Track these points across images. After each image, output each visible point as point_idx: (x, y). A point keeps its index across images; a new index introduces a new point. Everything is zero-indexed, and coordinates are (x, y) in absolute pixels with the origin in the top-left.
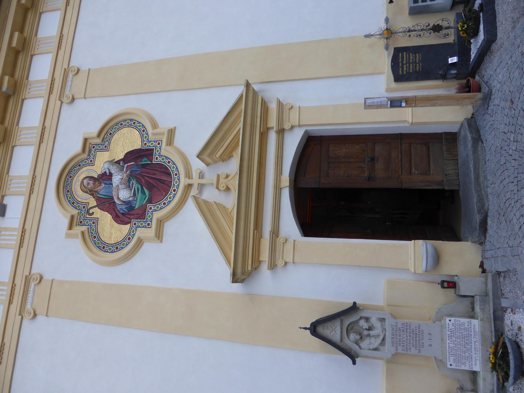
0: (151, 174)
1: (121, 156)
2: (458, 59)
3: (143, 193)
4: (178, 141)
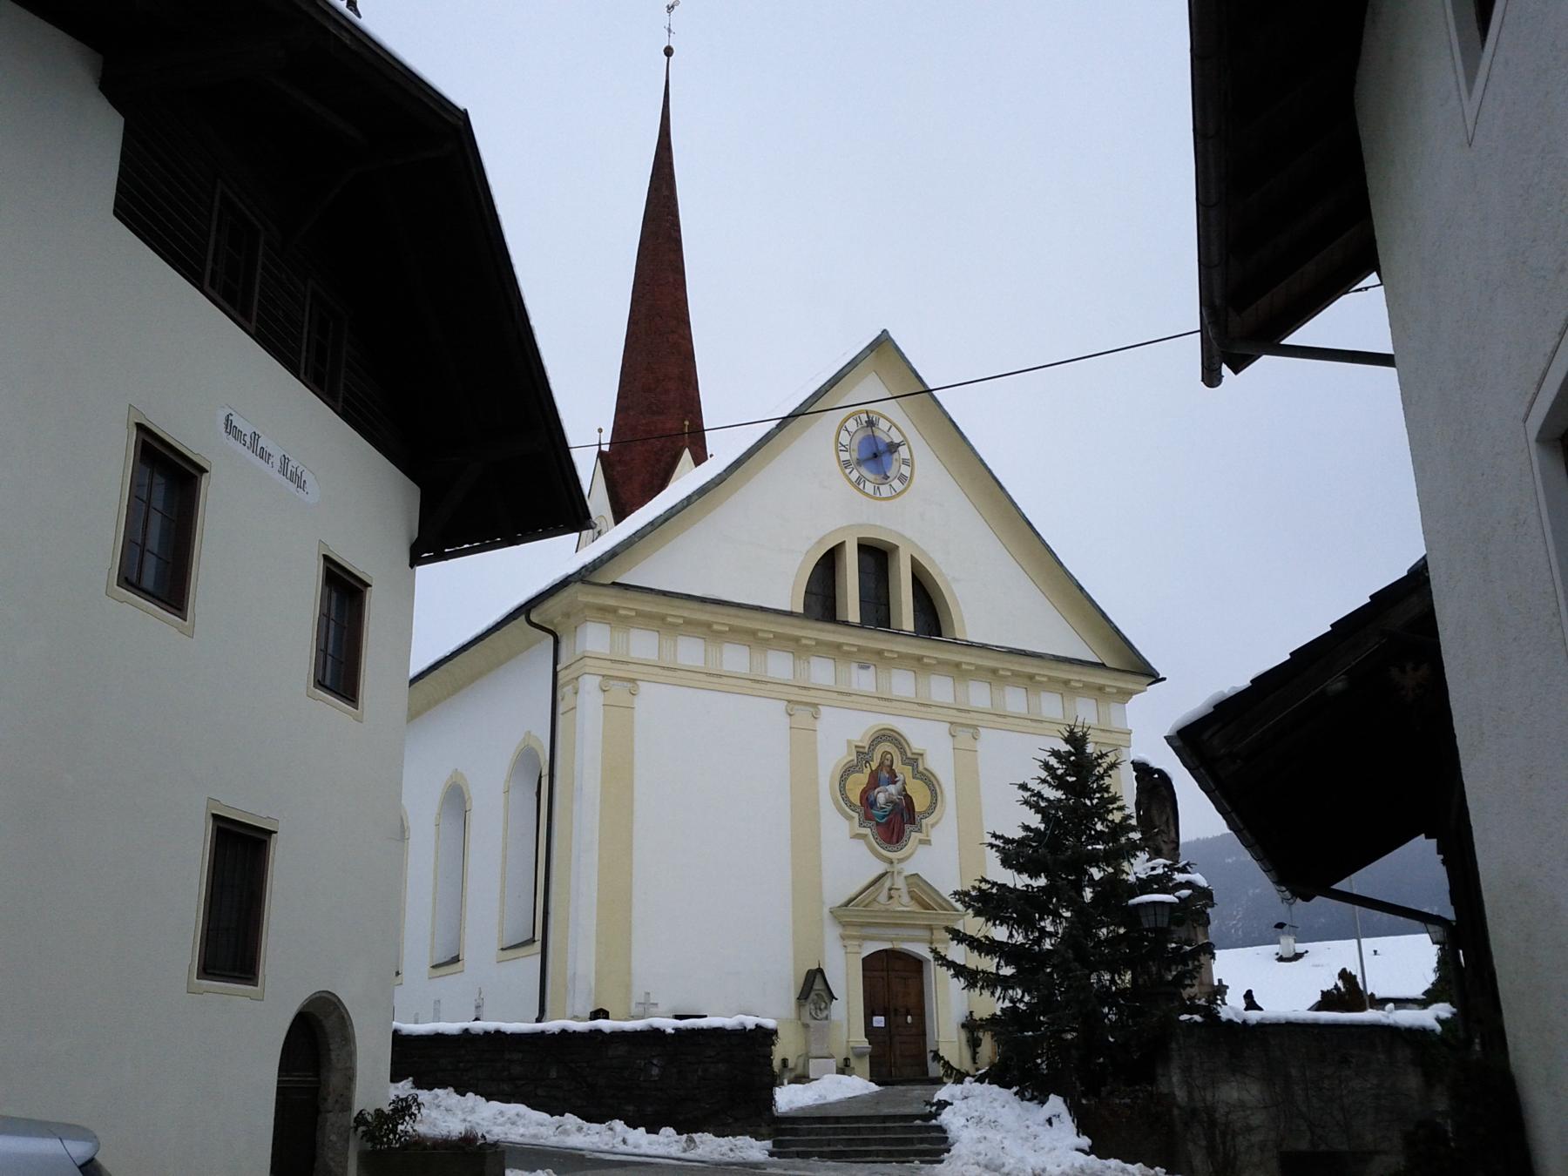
2: (771, 1100)
4: (922, 849)
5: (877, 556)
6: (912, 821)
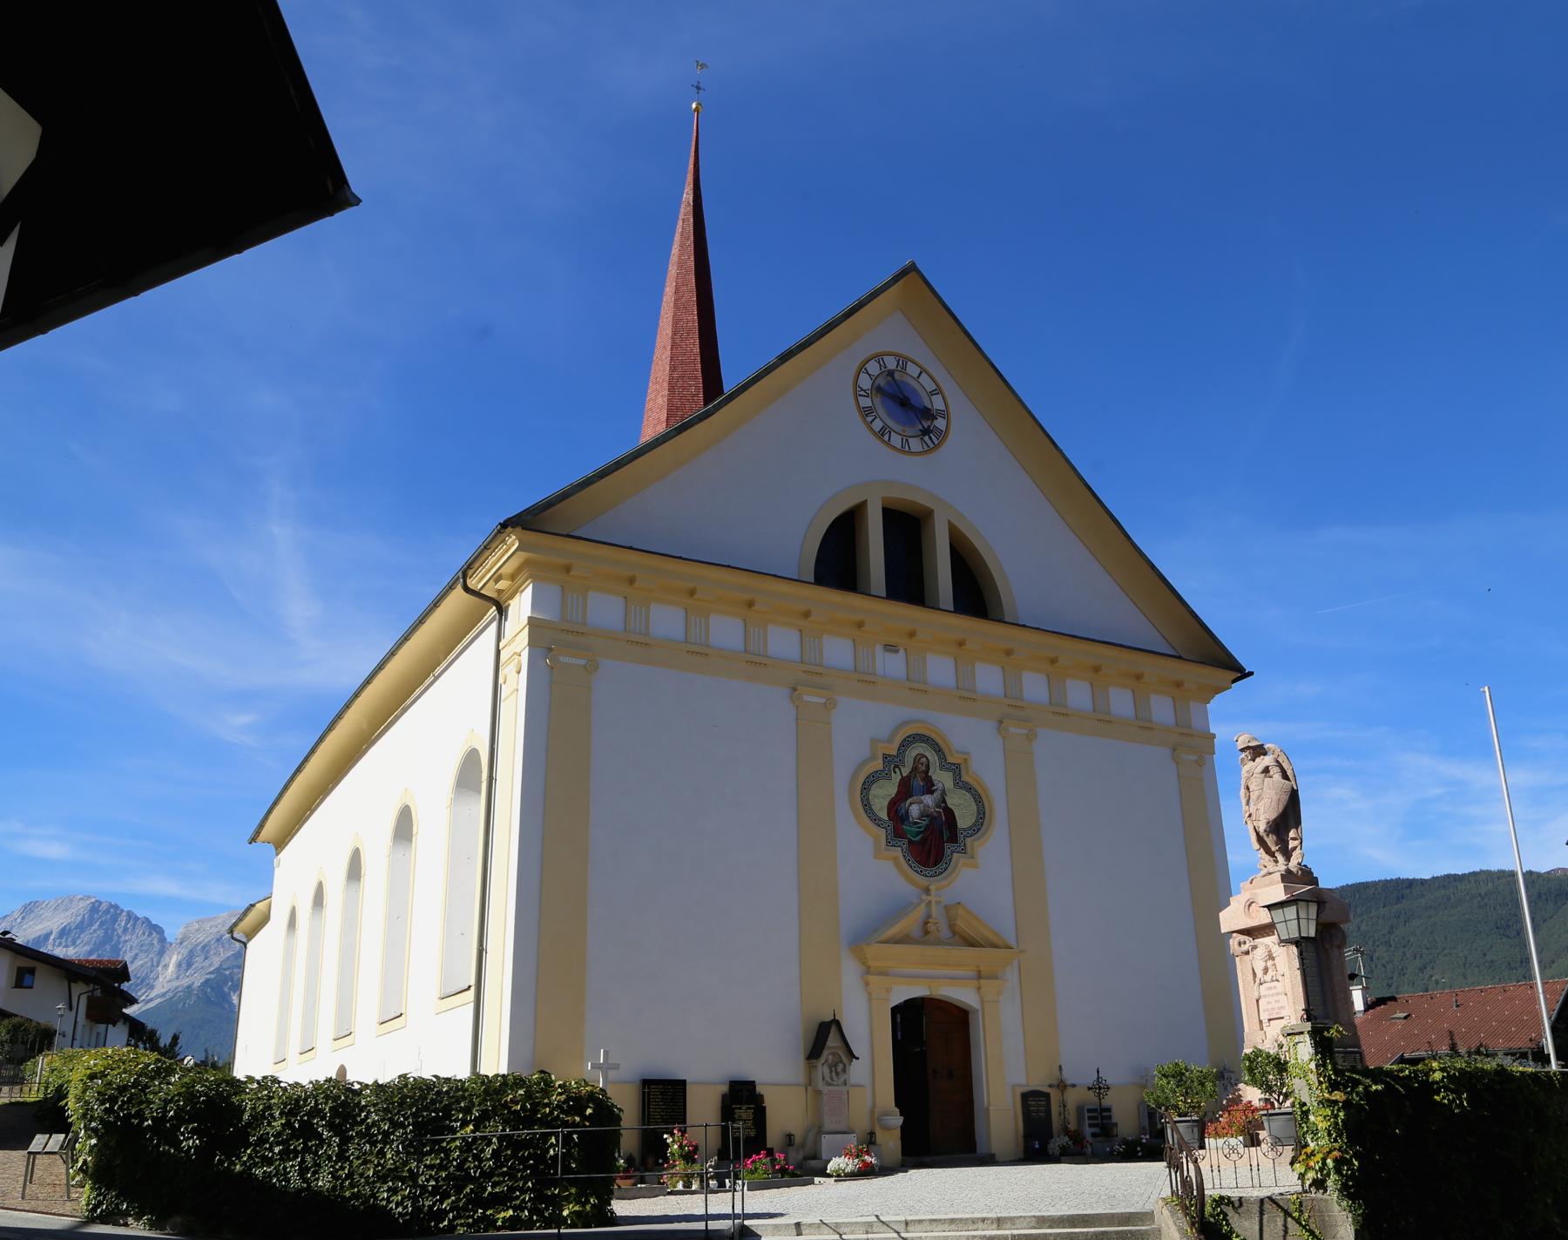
0: (931, 841)
1: (950, 803)
3: (918, 833)
5: (906, 526)
6: (954, 838)
